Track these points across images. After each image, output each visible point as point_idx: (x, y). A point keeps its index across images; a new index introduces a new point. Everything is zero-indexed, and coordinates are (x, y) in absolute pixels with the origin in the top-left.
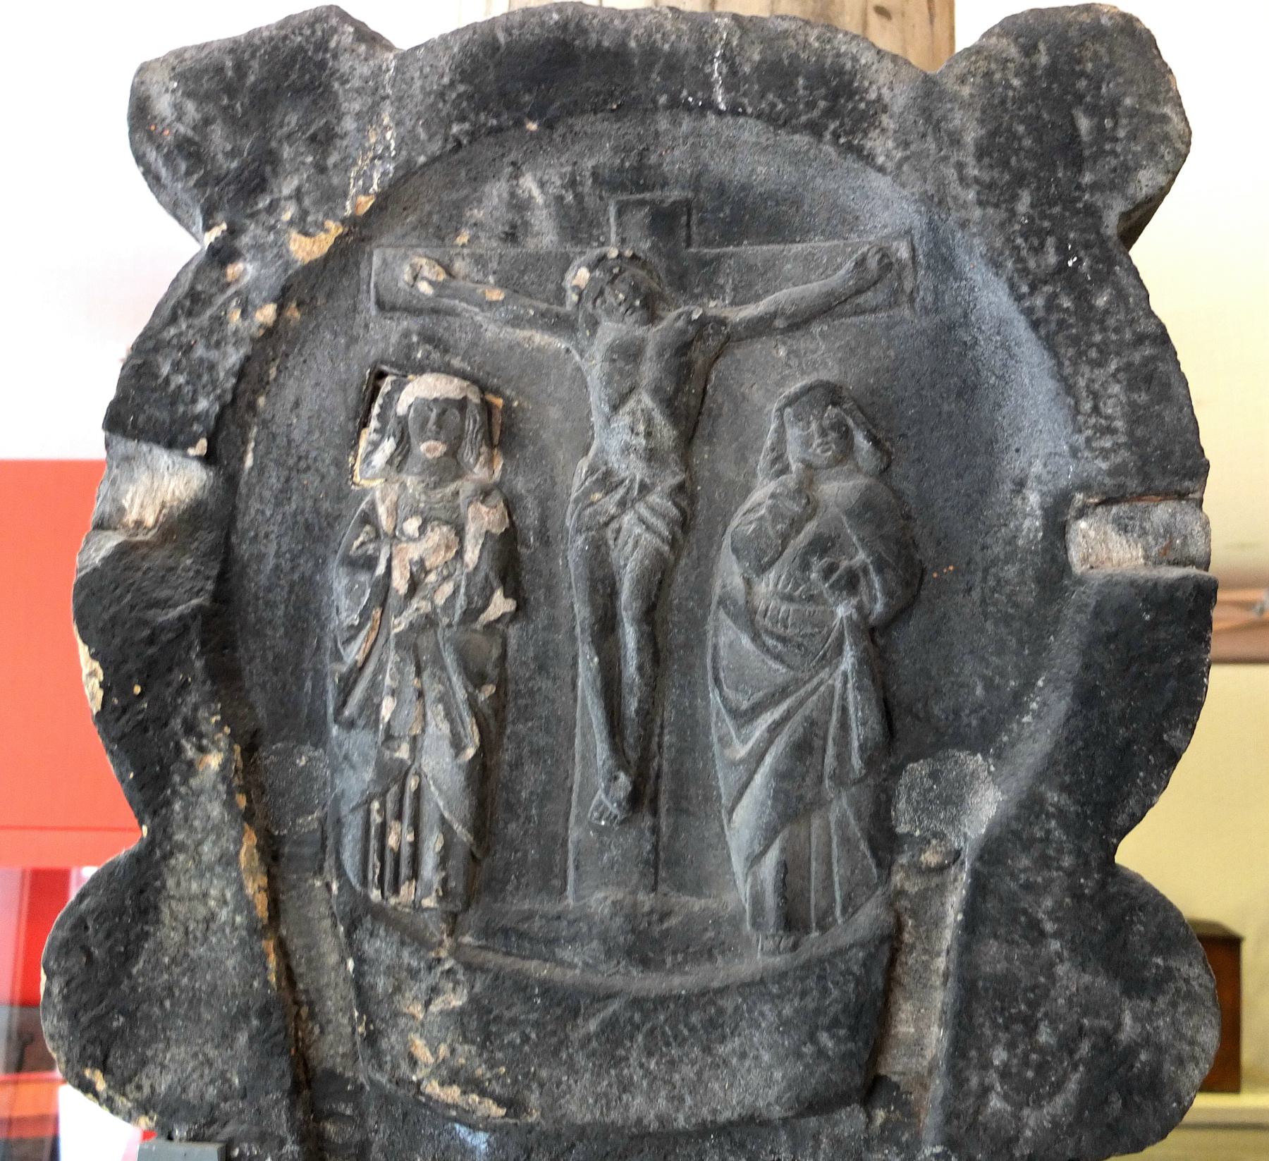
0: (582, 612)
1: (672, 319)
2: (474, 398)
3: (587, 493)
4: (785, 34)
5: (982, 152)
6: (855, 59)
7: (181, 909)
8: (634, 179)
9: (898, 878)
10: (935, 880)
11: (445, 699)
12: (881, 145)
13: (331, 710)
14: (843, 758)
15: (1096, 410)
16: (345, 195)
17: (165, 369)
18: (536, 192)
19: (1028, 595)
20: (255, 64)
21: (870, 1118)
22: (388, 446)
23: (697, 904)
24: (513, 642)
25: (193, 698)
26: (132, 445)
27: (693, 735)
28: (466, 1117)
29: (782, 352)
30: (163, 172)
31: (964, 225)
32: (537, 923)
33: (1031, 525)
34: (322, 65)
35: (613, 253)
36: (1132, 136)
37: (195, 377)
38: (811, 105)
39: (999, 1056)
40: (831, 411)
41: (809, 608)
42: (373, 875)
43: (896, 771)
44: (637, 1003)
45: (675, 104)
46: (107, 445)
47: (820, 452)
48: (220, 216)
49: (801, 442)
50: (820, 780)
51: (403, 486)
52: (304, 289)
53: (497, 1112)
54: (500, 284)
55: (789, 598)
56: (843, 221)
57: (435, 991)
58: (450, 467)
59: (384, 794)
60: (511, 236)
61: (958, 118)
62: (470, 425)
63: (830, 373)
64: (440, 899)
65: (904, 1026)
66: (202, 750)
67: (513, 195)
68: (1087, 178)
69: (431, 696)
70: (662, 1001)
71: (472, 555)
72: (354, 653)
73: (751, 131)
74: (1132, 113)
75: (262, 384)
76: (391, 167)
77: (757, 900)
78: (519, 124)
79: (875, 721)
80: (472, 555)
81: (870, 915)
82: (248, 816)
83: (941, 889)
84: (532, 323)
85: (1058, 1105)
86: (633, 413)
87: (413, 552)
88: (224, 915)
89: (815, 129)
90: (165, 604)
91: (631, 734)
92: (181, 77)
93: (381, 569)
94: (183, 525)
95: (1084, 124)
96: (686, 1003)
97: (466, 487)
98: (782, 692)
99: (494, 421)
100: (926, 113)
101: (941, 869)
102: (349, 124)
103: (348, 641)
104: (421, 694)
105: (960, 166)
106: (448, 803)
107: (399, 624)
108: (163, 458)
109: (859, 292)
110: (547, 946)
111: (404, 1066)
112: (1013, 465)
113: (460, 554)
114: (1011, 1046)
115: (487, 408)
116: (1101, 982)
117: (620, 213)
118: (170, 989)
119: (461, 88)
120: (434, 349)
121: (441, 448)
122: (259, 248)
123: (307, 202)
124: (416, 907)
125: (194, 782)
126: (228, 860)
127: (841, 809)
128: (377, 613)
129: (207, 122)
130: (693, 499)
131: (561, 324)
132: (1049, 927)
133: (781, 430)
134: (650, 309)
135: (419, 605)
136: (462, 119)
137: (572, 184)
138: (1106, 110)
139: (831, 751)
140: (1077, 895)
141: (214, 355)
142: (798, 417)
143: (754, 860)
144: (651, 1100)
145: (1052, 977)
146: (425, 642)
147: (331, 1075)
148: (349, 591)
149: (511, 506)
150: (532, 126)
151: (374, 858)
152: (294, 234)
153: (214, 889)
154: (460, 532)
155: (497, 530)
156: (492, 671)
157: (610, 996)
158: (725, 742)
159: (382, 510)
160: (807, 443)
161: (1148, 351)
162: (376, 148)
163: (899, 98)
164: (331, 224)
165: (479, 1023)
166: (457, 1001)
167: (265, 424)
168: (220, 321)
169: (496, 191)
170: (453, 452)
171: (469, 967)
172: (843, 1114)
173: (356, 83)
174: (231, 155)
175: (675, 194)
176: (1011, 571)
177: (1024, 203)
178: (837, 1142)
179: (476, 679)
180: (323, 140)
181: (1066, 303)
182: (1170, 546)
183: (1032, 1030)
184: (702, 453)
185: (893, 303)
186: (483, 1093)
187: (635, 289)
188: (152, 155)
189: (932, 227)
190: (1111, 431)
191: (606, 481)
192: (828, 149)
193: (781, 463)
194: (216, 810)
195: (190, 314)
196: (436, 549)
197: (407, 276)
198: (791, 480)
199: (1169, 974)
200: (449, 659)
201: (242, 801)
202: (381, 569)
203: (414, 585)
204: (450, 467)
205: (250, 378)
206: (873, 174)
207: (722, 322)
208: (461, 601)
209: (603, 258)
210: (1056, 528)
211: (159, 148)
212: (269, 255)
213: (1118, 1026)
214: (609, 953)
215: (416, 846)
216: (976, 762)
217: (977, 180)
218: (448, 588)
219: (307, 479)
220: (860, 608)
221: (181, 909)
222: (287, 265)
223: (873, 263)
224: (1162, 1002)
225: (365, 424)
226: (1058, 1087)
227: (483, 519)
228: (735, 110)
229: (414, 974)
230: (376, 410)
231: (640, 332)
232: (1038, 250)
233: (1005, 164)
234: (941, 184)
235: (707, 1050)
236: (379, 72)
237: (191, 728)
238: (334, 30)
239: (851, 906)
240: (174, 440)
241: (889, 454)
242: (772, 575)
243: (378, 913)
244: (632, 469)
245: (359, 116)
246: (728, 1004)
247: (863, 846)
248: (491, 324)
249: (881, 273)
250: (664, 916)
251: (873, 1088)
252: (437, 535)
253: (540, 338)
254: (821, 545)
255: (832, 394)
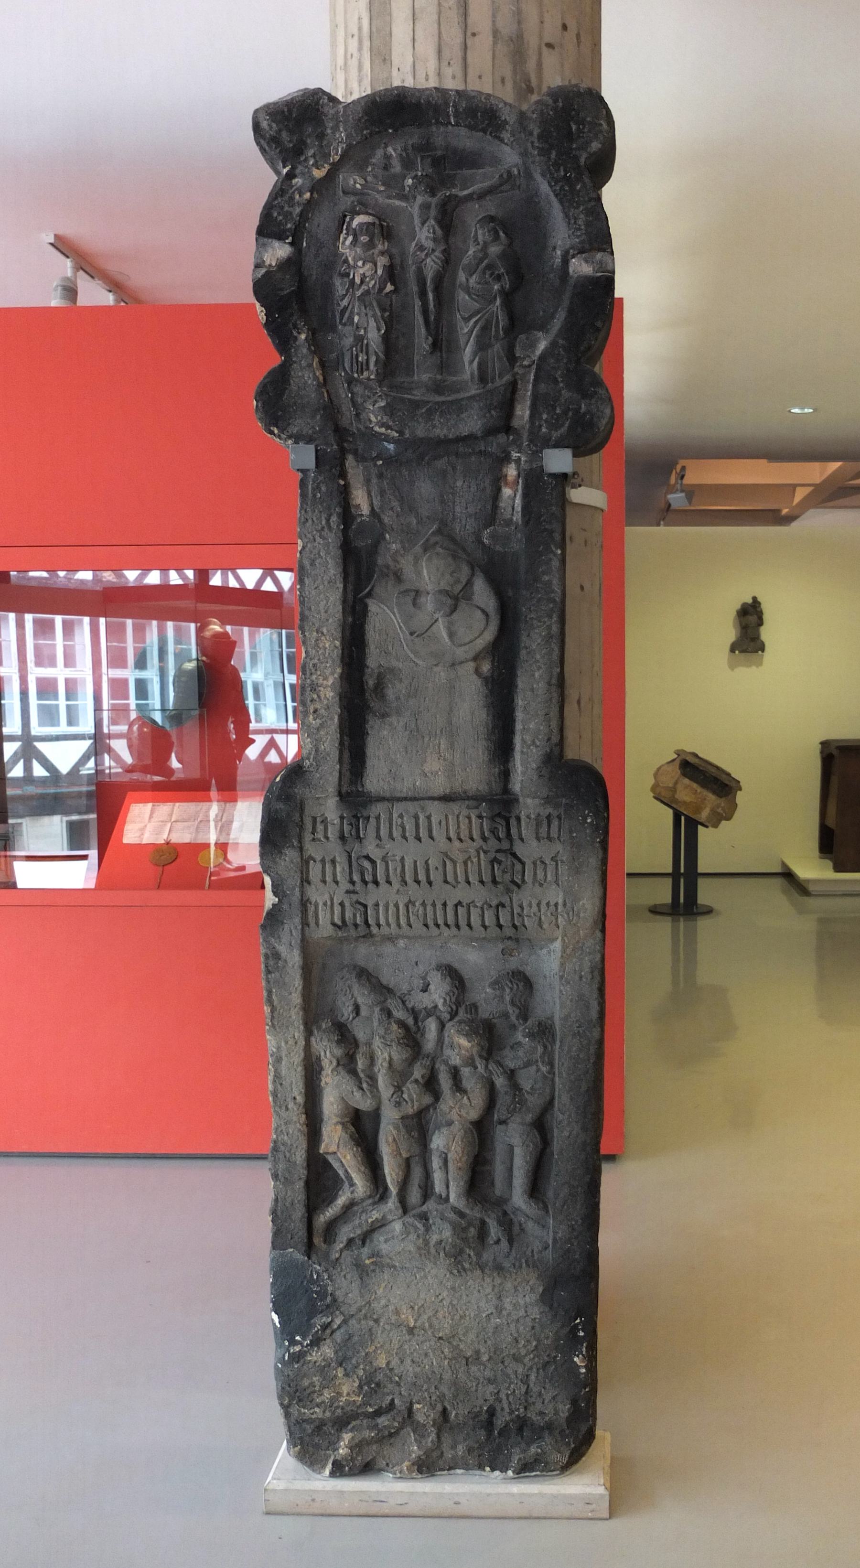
0: (415, 289)
1: (441, 195)
2: (377, 222)
3: (415, 252)
4: (474, 97)
5: (540, 137)
6: (497, 105)
7: (297, 380)
8: (424, 148)
9: (516, 370)
10: (527, 369)
11: (374, 316)
12: (506, 136)
13: (338, 321)
14: (497, 331)
15: (575, 223)
16: (330, 155)
17: (275, 214)
18: (393, 153)
19: (557, 282)
20: (295, 110)
21: (508, 438)
22: (350, 238)
23: (455, 379)
24: (394, 300)
25: (295, 318)
26: (266, 240)
27: (452, 328)
28: (388, 439)
29: (477, 206)
30: (267, 148)
31: (533, 162)
32: (406, 384)
33: (558, 261)
34: (318, 110)
35: (420, 174)
36: (590, 131)
37: (285, 217)
38: (483, 122)
39: (545, 416)
40: (491, 224)
41: (486, 286)
42: (355, 369)
43: (515, 338)
44: (437, 403)
45: (438, 123)
46: (257, 240)
47: (488, 238)
48: (288, 163)
49: (482, 235)
50: (490, 339)
51: (356, 252)
52: (317, 187)
53: (396, 435)
54: (383, 185)
55: (479, 283)
56: (495, 161)
57: (376, 402)
58: (370, 245)
59: (356, 345)
60: (386, 168)
61: (531, 126)
62: (376, 231)
63: (493, 213)
64: (376, 376)
65: (518, 412)
66: (299, 333)
67: (385, 154)
68: (574, 146)
69: (369, 315)
70: (443, 403)
71: (380, 272)
72: (345, 303)
73: (463, 131)
74: (590, 123)
75: (307, 220)
76: (344, 146)
77: (472, 374)
78: (386, 130)
79: (506, 320)
80: (380, 272)
81: (507, 378)
82: (315, 353)
83: (529, 372)
84: (394, 197)
85: (563, 430)
86: (544, 1032)
87: (361, 271)
88: (310, 382)
89: (484, 131)
90: (282, 289)
91: (432, 327)
92: (270, 114)
93: (351, 276)
94: (285, 265)
95: (574, 127)
96: (451, 402)
97: (376, 251)
98: (478, 312)
99: (384, 229)
100: (521, 124)
101: (530, 366)
102: (329, 131)
103: (342, 300)
104: (366, 315)
105: (532, 143)
106: (377, 347)
107: (358, 293)
108: (276, 244)
109: (501, 185)
110: (409, 390)
111: (368, 423)
112: (551, 242)
113: (376, 272)
114: (548, 414)
115: (381, 226)
116: (575, 395)
117: (421, 160)
118: (295, 403)
119: (366, 118)
120: (363, 206)
121: (368, 239)
122: (303, 174)
123: (317, 158)
124: (369, 379)
125: (297, 343)
126: (310, 365)
127: (497, 348)
128: (351, 290)
129: (280, 130)
130: (449, 254)
131: (404, 197)
132: (560, 379)
133: (476, 231)
134: (433, 192)
135: (364, 287)
136: (367, 129)
137: (405, 149)
138: (582, 122)
139: (493, 329)
140: (568, 370)
141: (291, 209)
142: (481, 227)
143: (471, 362)
144: (442, 429)
145: (561, 394)
146: (367, 298)
147: (345, 429)
148: (341, 284)
149: (391, 257)
150: (390, 131)
151: (355, 365)
152: (314, 169)
153: (306, 375)
154: (375, 265)
155: (388, 264)
156: (388, 308)
157: (428, 402)
158: (462, 329)
159: (350, 259)
160: (484, 235)
161: (593, 203)
162: (339, 140)
163: (511, 118)
164: (326, 165)
165: (390, 410)
166: (383, 404)
167: (309, 232)
168: (292, 198)
169: (379, 153)
170: (371, 240)
171: (386, 395)
172: (500, 436)
173: (330, 116)
174: (290, 141)
175: (439, 153)
176: (552, 276)
177: (553, 156)
178: (498, 444)
179: (383, 310)
180: (321, 136)
181: (567, 188)
182: (601, 267)
183: (554, 409)
184: (452, 240)
185: (513, 189)
186: (392, 430)
187: (427, 186)
188: (262, 142)
189: (524, 164)
190: (579, 229)
191: (421, 248)
192: (488, 137)
193: (477, 240)
194: (305, 351)
195: (282, 196)
196: (368, 270)
197: (352, 182)
198: (479, 247)
199: (595, 393)
200: (375, 304)
201: (313, 348)
202: (351, 276)
203: (362, 282)
204: (370, 245)
205: (304, 216)
206: (503, 145)
207: (456, 196)
208: (377, 286)
209: (416, 176)
210: (565, 261)
211: (265, 139)
212: (307, 176)
213: (580, 408)
214: (428, 390)
215: (367, 360)
216: (540, 334)
217: (538, 148)
218: (373, 282)
219: (323, 250)
220: (502, 286)
221: (297, 380)
222: (313, 179)
223: (505, 176)
224: (593, 401)
225: (341, 232)
226: (563, 425)
227: (382, 261)
228: (457, 124)
229: (369, 397)
230: (345, 227)
231: (430, 199)
232: (558, 171)
233: (547, 142)
234: (526, 150)
235: (458, 416)
236: (338, 112)
237: (295, 326)
238: (321, 98)
239: (501, 376)
240: (281, 237)
241: (511, 238)
242: (474, 277)
243: (357, 380)
244: (429, 244)
245: (332, 128)
246: (464, 403)
247: (505, 359)
248: (380, 197)
249: (508, 178)
250: (444, 381)
251: (508, 429)
252: (368, 266)
253: (397, 203)
254: (489, 267)
255: (492, 219)
